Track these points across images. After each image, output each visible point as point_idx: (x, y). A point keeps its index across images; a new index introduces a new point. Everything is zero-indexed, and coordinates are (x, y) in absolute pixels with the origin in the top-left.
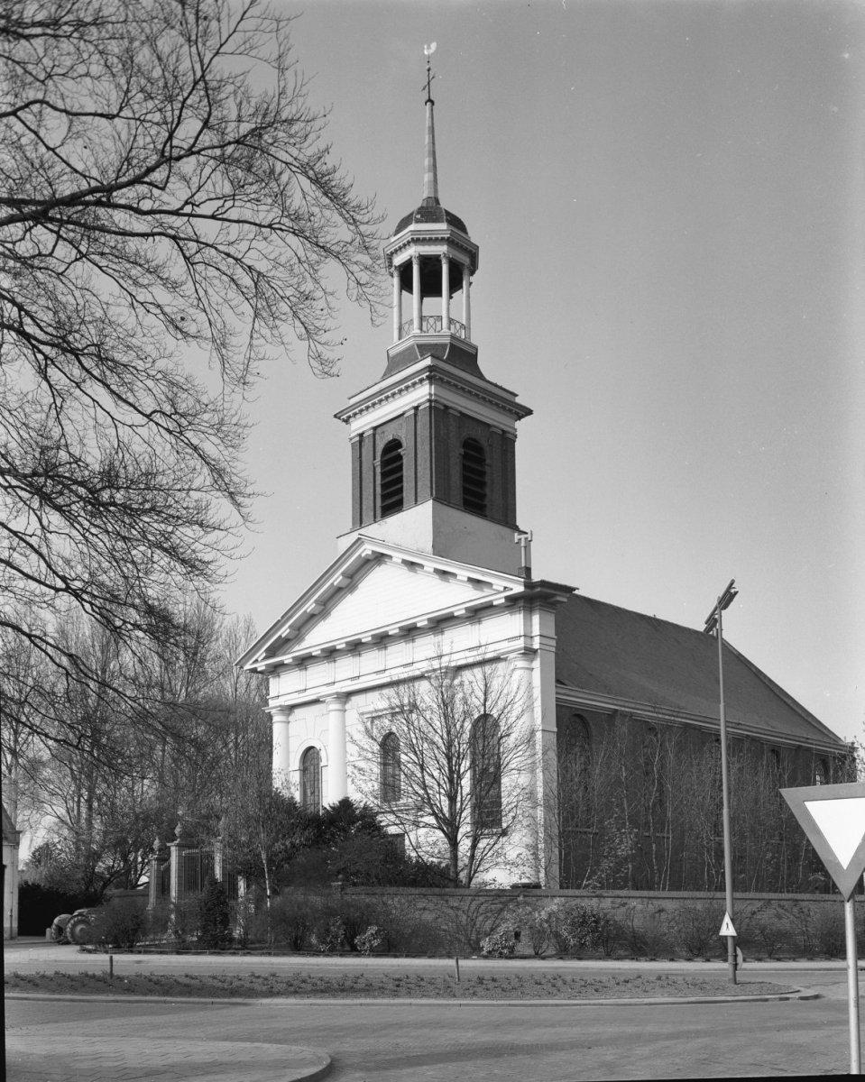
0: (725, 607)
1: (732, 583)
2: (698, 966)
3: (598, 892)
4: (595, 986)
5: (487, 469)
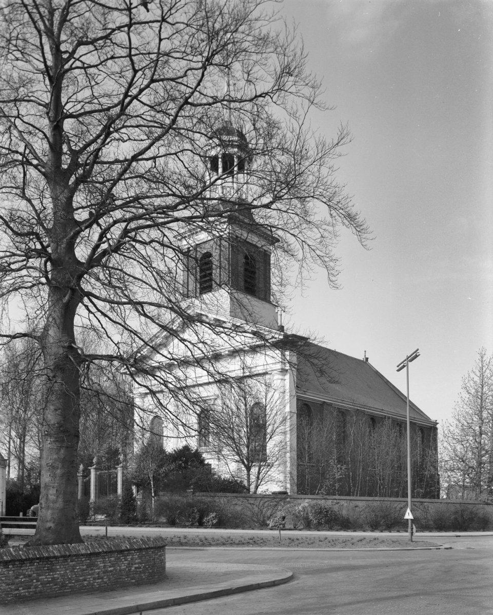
0: (411, 361)
1: (418, 350)
2: (394, 534)
3: (325, 497)
4: (333, 542)
5: (257, 271)
